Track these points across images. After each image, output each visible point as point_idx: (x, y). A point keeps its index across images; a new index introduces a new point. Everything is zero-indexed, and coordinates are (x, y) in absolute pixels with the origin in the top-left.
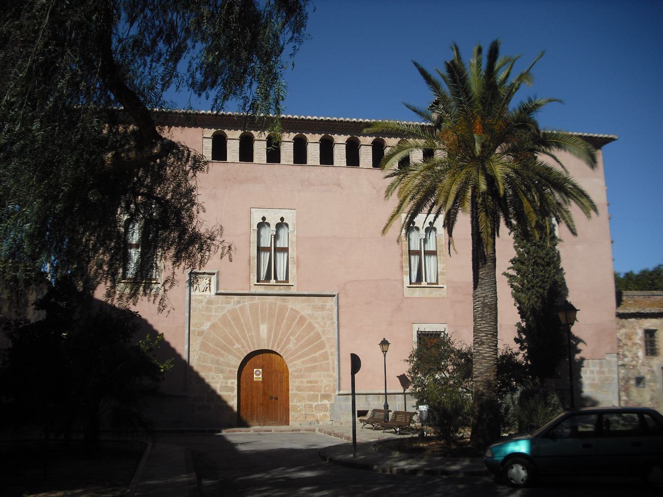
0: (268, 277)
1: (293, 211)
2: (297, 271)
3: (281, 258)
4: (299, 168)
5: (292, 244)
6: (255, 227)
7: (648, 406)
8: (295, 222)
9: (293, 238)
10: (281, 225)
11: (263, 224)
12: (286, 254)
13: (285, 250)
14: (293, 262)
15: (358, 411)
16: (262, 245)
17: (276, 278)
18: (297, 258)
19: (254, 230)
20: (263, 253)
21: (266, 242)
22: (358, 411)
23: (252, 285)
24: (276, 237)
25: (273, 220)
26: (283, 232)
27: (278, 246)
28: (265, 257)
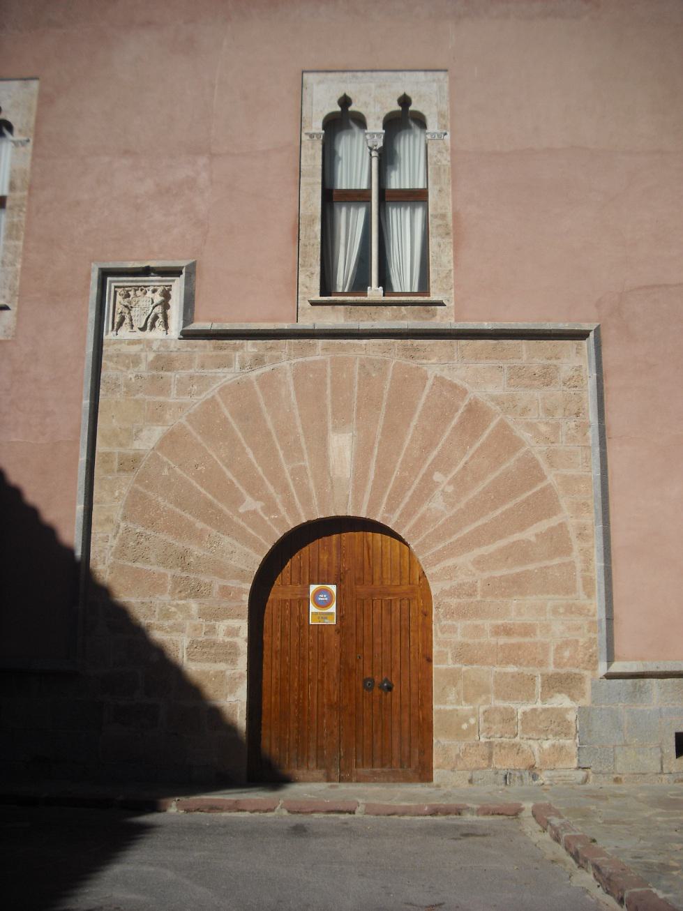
0: (360, 283)
1: (441, 75)
2: (456, 258)
6: (317, 127)
8: (445, 107)
10: (403, 119)
11: (343, 120)
12: (419, 213)
13: (416, 197)
17: (384, 281)
18: (456, 216)
19: (311, 136)
20: (344, 210)
23: (303, 304)
24: (386, 158)
25: (375, 104)
26: (409, 146)
28: (351, 222)
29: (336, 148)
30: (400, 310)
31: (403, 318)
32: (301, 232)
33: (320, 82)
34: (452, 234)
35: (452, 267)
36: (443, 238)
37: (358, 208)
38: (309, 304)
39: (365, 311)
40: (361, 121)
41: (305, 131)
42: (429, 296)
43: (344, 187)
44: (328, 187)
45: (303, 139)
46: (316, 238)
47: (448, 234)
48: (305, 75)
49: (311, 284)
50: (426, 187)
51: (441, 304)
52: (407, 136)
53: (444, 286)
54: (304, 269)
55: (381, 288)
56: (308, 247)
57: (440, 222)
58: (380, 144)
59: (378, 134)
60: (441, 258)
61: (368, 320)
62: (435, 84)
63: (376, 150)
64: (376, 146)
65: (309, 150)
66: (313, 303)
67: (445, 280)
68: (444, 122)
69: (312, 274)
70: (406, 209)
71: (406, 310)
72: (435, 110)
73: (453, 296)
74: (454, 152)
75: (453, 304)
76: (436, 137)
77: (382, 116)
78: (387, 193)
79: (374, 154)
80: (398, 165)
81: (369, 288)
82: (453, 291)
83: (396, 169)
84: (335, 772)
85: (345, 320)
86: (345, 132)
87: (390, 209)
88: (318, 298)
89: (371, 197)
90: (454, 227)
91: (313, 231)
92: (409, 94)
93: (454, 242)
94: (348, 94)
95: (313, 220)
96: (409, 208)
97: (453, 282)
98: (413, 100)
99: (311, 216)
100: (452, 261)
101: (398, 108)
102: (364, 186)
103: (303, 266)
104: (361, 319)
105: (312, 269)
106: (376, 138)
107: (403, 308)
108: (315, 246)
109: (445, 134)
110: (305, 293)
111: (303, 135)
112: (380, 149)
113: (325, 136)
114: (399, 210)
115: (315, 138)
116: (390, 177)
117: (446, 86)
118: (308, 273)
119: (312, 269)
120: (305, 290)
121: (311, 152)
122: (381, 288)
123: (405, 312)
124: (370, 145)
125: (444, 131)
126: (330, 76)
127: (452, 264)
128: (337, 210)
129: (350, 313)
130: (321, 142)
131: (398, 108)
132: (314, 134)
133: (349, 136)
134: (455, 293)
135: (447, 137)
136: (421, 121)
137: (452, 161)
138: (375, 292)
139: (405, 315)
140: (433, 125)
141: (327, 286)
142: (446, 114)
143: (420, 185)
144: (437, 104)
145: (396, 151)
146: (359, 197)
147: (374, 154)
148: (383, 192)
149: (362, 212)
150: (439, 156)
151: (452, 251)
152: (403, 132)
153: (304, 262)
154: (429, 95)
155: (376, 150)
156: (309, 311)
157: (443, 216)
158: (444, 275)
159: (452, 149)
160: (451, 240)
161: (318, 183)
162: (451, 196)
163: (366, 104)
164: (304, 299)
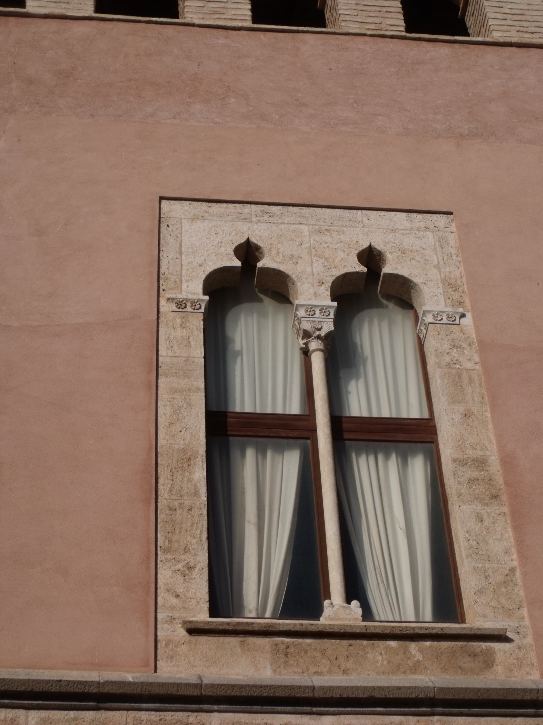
0: (303, 591)
1: (441, 220)
2: (520, 543)
3: (392, 492)
4: (436, 54)
5: (457, 379)
6: (194, 289)
7: (114, 692)
8: (456, 272)
9: (455, 349)
10: (370, 288)
11: (244, 283)
12: (418, 467)
13: (412, 435)
14: (480, 489)
15: (211, 616)
16: (245, 400)
17: (355, 589)
18: (507, 462)
19: (181, 304)
20: (250, 454)
21: (271, 370)
22: (211, 616)
23: (172, 632)
24: (340, 355)
25: (313, 256)
26: (381, 338)
27: (357, 406)
28: (270, 483)
29: (229, 332)
30: (406, 651)
31: (415, 668)
32: (161, 481)
33: (195, 218)
34: (504, 498)
35: (515, 563)
36: (486, 505)
37: (280, 450)
38: (183, 633)
39: (323, 652)
40: (278, 288)
41: (165, 296)
42: (463, 621)
43: (248, 409)
44: (214, 408)
45: (162, 309)
46: (196, 493)
47: (495, 497)
48: (164, 202)
49: (193, 596)
50: (426, 416)
51: (501, 638)
52: (376, 321)
53: (504, 601)
54: (169, 556)
55: (355, 603)
56: (179, 511)
57: (475, 474)
58: (328, 326)
59: (323, 309)
60: (487, 543)
61: (330, 672)
62: (429, 234)
63: (319, 337)
64: (319, 330)
65: (175, 329)
66: (194, 631)
67: (504, 590)
68: (456, 296)
69: (190, 568)
70: (387, 457)
71: (420, 651)
72: (434, 274)
73: (527, 622)
74: (483, 346)
75: (529, 640)
76: (445, 320)
77: (329, 281)
78: (345, 426)
79: (314, 345)
80: (362, 369)
81: (326, 603)
82: (525, 612)
83: (357, 378)
84: (260, 255)
85: (275, 671)
86: (245, 306)
87: (354, 456)
88: (202, 616)
89: (314, 430)
90: (506, 482)
91: (190, 480)
92: (378, 245)
93: (513, 513)
94: (253, 240)
95: (189, 459)
96: (394, 456)
97: (522, 593)
98: (389, 256)
99: (184, 450)
100: (513, 550)
101: (356, 267)
102: (295, 408)
103: (167, 551)
104: (313, 669)
105: (189, 558)
106: (318, 314)
107: (413, 647)
108: (196, 512)
109: (463, 316)
110: (173, 608)
111: (163, 302)
112: (329, 335)
113: (210, 305)
114: (372, 459)
115: (189, 309)
116: (348, 393)
117: (453, 239)
118: (179, 566)
119: (189, 558)
120: (174, 601)
121: (180, 333)
122: (355, 603)
123: (419, 657)
124: (307, 326)
125: (461, 310)
126: (216, 208)
127: (515, 557)
128: (235, 453)
129: (286, 655)
130: (201, 317)
131: (356, 267)
132: (187, 300)
133: (255, 316)
134: (531, 616)
135: (468, 321)
136: (401, 294)
137: (483, 363)
138: (338, 610)
139: (418, 661)
140: (431, 299)
141: (223, 593)
142: (459, 282)
143: (414, 410)
144: (437, 266)
145: (354, 345)
146: (292, 430)
147: (314, 345)
148: (339, 424)
149: (290, 463)
150: (455, 353)
151: (509, 530)
152: (366, 314)
153: (170, 541)
154: (414, 250)
155: (319, 337)
156: (184, 648)
157: (481, 463)
158: (501, 578)
159: (481, 343)
160: (506, 509)
161: (198, 389)
162: (491, 426)
163: (294, 259)
164: (171, 620)
